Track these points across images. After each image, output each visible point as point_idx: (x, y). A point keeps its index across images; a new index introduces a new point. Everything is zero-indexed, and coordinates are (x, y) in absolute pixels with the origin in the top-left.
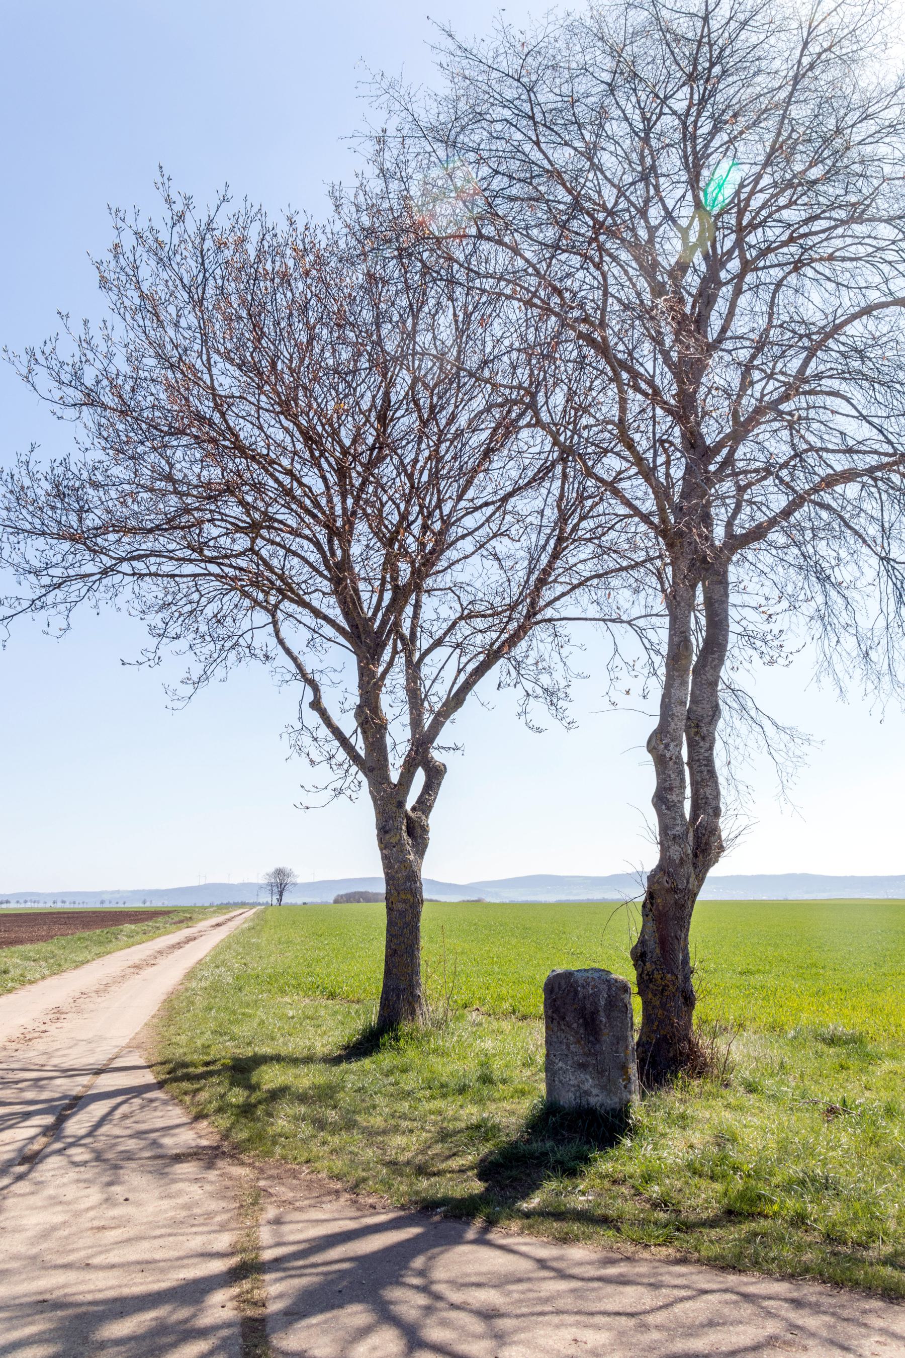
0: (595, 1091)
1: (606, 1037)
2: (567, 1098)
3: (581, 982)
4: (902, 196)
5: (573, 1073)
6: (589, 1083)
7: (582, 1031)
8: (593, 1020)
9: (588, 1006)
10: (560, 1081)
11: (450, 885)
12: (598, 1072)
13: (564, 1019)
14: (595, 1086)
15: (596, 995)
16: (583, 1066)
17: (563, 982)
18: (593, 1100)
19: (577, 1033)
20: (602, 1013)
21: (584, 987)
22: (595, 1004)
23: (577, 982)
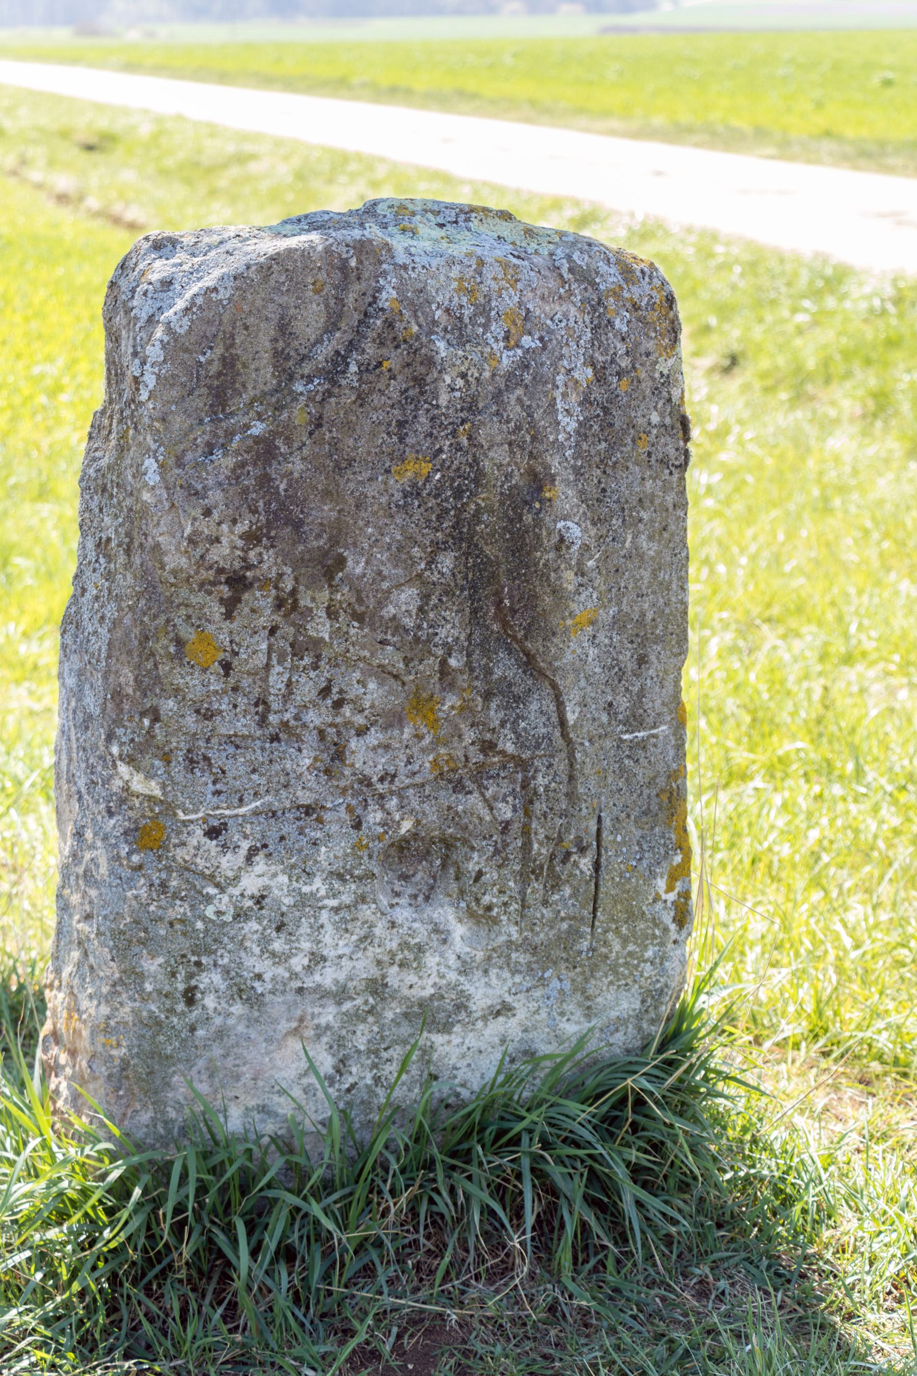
0: (482, 993)
1: (580, 649)
2: (279, 1080)
3: (444, 293)
4: (911, 777)
5: (344, 916)
6: (447, 947)
7: (451, 628)
8: (521, 543)
9: (497, 457)
10: (242, 991)
11: (223, 78)
12: (529, 871)
13: (329, 567)
14: (498, 957)
15: (529, 375)
16: (422, 859)
17: (310, 319)
18: (470, 1058)
19: (417, 645)
20: (564, 495)
21: (460, 333)
22: (529, 438)
23: (418, 301)
